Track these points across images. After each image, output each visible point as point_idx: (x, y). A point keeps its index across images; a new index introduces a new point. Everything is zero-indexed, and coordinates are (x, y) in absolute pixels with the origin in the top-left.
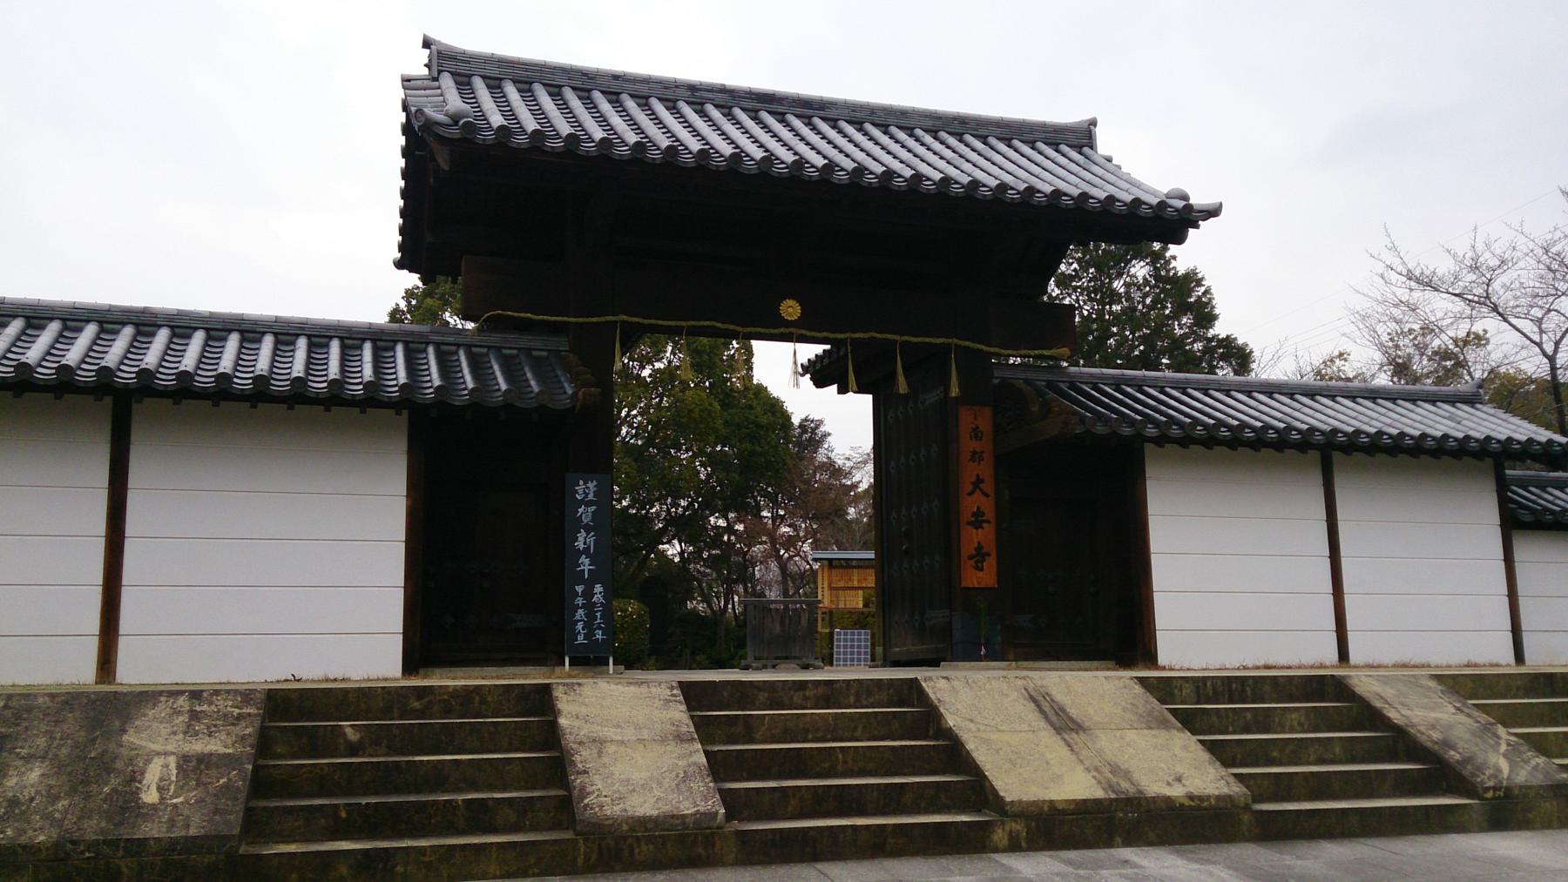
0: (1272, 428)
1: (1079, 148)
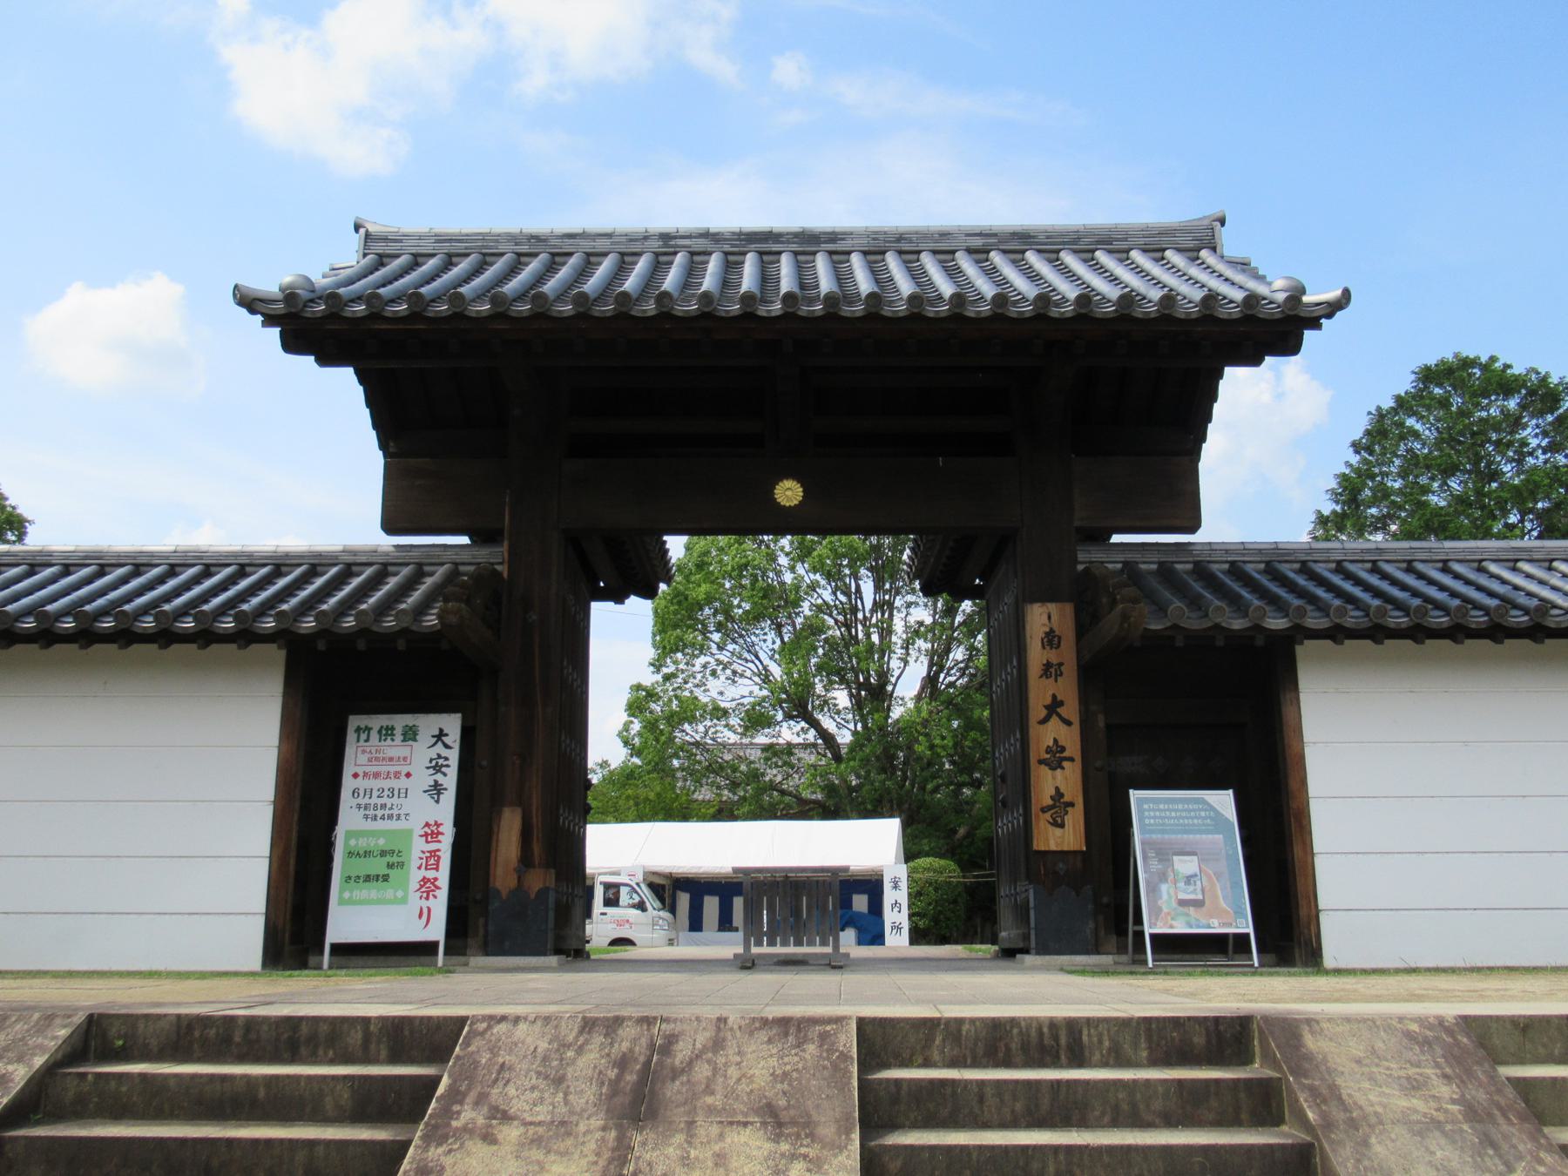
0: (1477, 606)
1: (1192, 254)
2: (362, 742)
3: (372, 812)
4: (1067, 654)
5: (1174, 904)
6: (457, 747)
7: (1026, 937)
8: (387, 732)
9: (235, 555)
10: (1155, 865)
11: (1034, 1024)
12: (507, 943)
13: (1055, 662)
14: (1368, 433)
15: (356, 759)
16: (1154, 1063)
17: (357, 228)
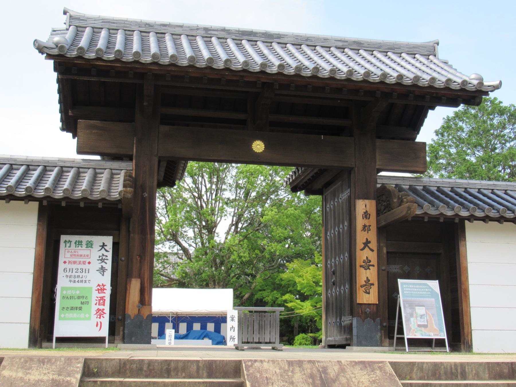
1: (427, 56)
2: (67, 248)
3: (73, 279)
4: (373, 222)
5: (416, 327)
6: (111, 251)
7: (351, 339)
8: (79, 243)
9: (26, 160)
10: (409, 311)
11: (449, 364)
12: (133, 339)
13: (368, 225)
14: (443, 127)
15: (65, 255)
16: (490, 379)
17: (65, 13)
